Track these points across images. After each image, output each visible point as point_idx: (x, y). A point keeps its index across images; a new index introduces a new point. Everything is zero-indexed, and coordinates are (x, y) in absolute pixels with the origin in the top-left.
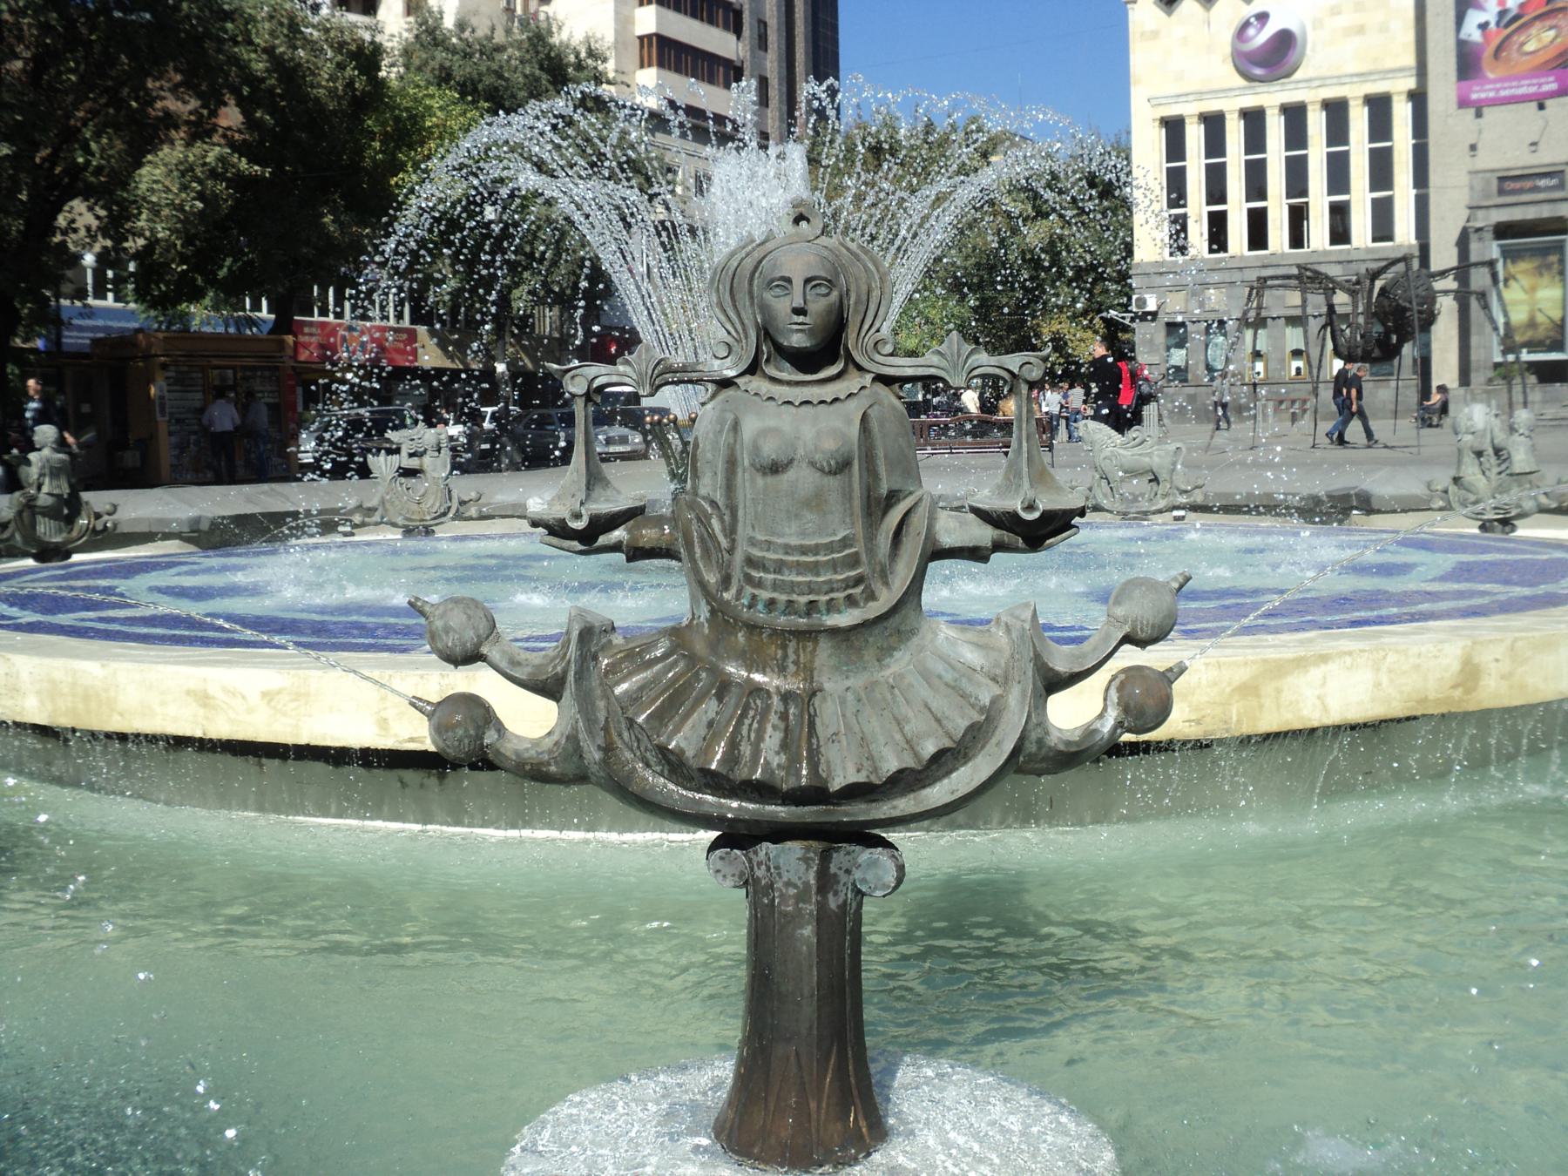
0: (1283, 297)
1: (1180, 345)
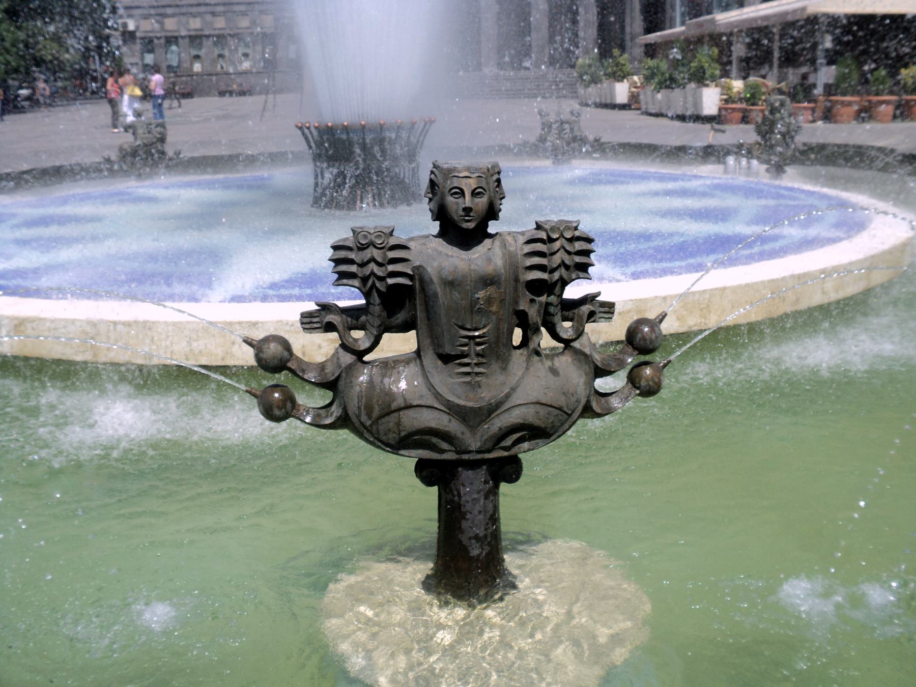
0: (188, 23)
1: (151, 51)
